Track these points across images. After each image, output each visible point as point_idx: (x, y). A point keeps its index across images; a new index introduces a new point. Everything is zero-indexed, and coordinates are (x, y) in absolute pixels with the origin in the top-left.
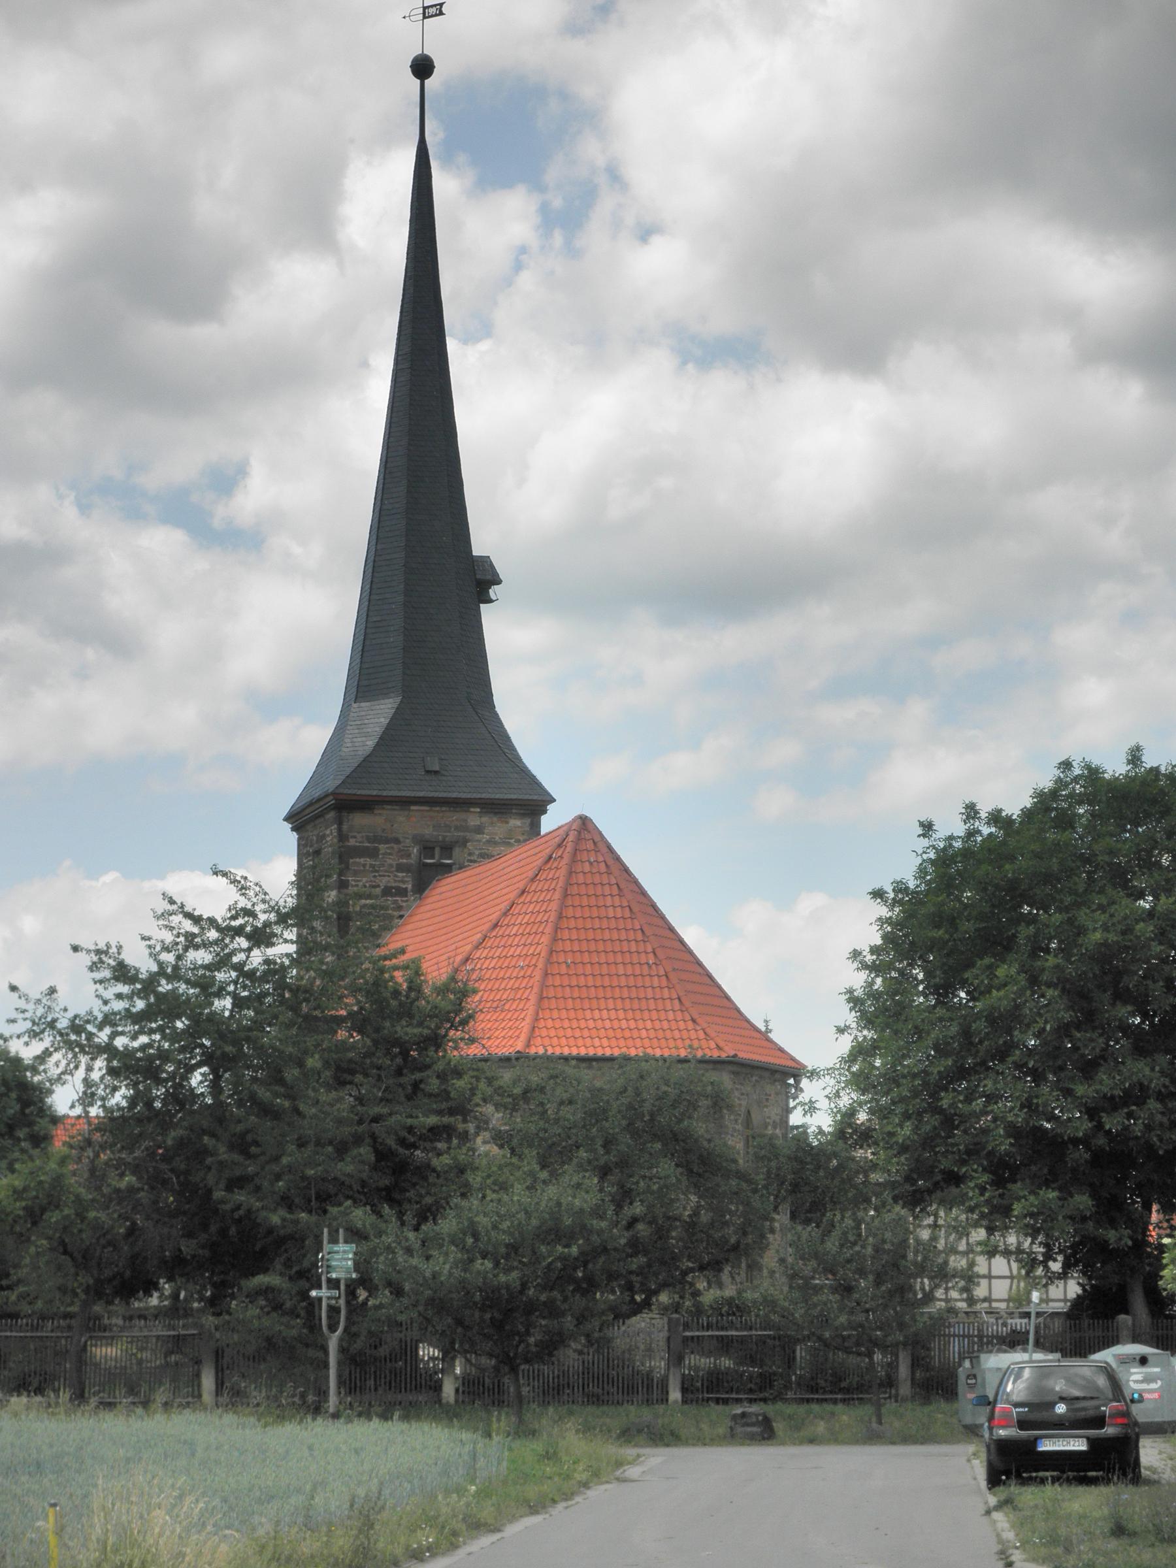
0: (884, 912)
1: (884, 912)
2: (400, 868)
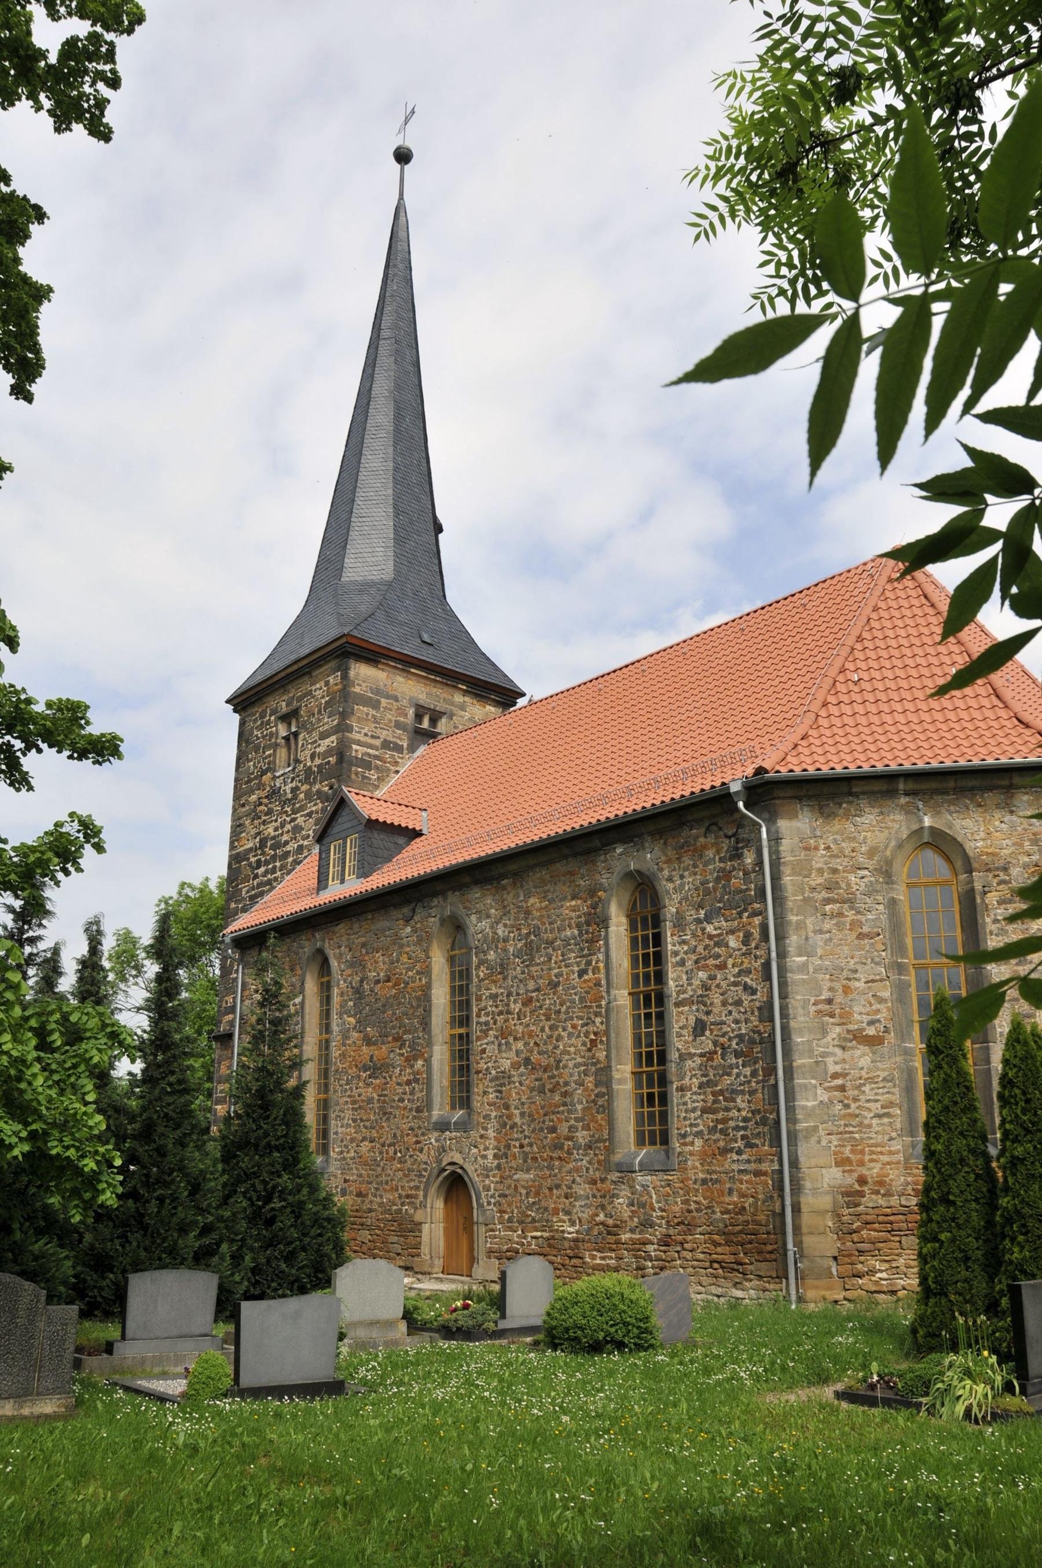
0: (148, 995)
1: (148, 995)
2: (398, 725)
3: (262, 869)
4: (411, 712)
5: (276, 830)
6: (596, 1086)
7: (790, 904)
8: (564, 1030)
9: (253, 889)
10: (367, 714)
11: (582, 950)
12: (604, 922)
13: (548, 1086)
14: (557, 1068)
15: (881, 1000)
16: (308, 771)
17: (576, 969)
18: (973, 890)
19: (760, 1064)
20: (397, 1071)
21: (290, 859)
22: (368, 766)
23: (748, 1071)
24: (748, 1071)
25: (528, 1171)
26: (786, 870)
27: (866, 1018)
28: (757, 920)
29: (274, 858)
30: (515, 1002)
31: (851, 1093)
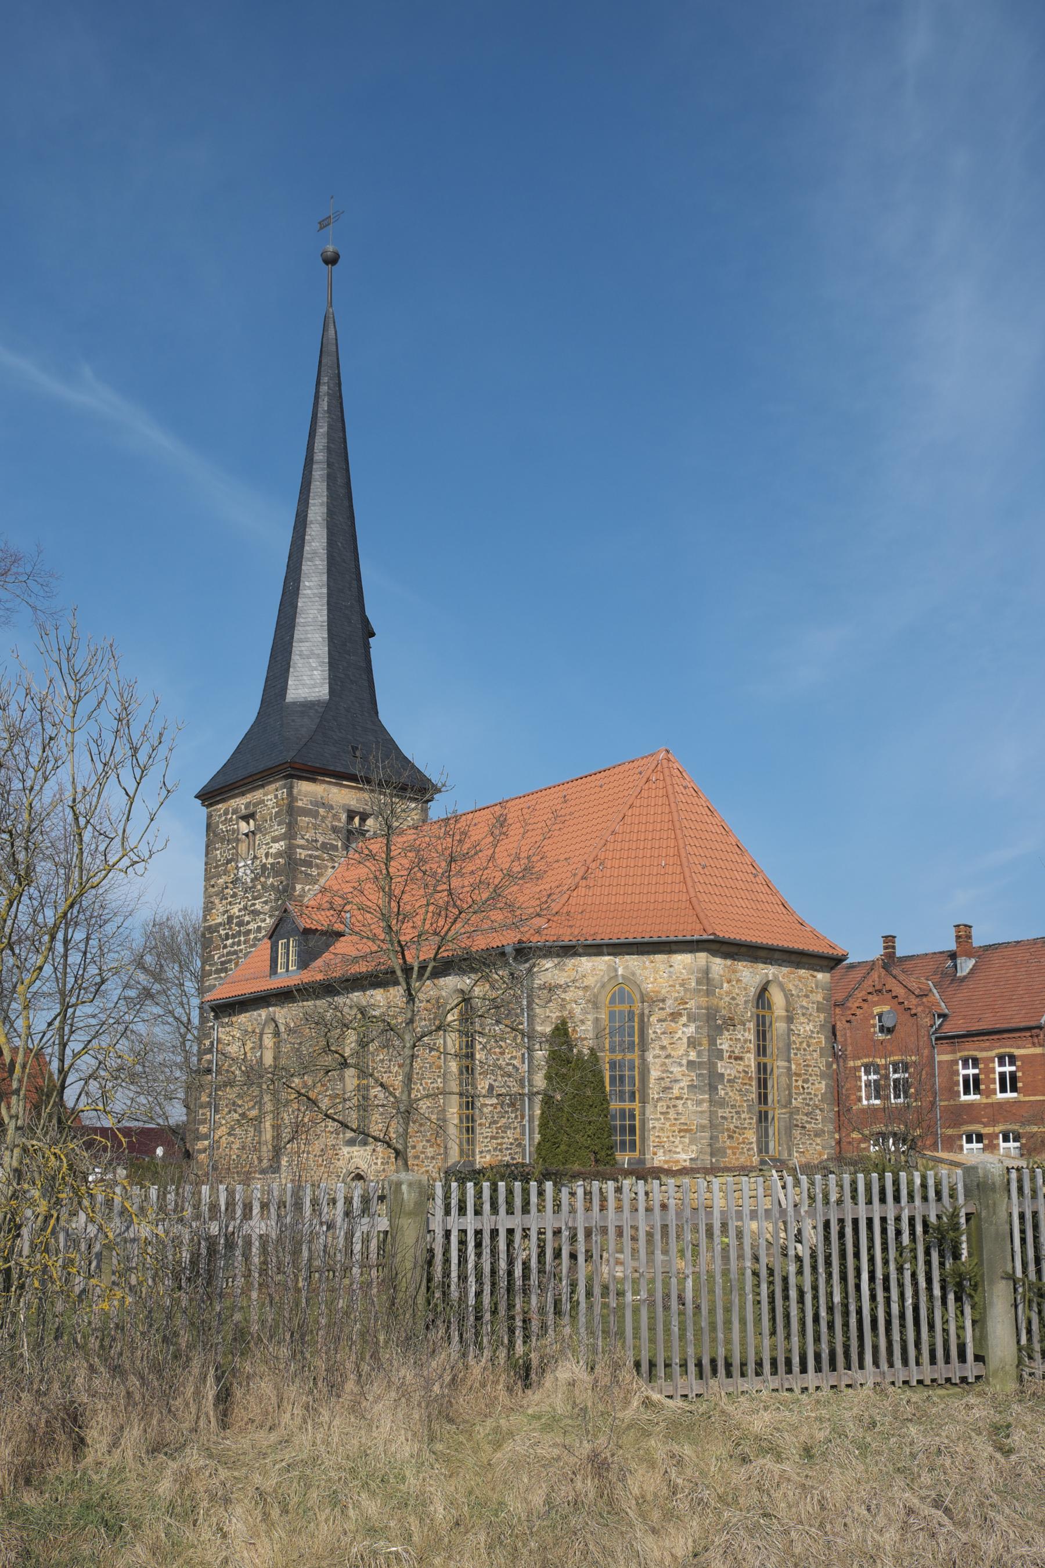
3: (230, 941)
4: (344, 817)
5: (240, 911)
9: (223, 956)
10: (308, 823)
12: (227, 1204)
16: (264, 867)
19: (518, 1113)
21: (252, 936)
22: (309, 865)
23: (513, 1115)
24: (513, 1115)
29: (239, 933)
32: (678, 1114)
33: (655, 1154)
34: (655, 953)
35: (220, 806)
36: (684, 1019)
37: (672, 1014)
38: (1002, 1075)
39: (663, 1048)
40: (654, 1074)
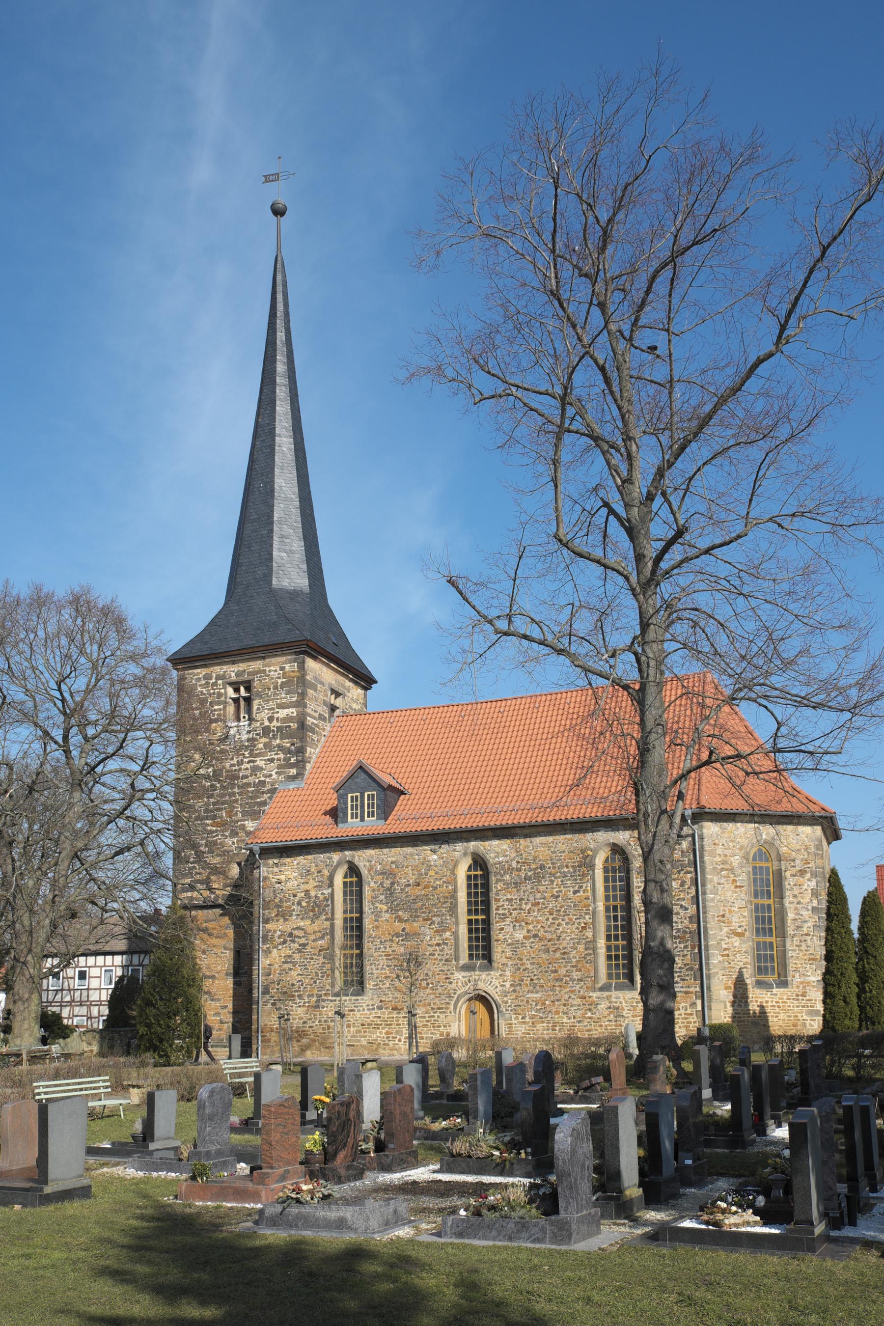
6: (586, 949)
7: (707, 870)
8: (563, 920)
11: (576, 880)
13: (551, 949)
14: (558, 940)
15: (745, 917)
17: (572, 889)
18: (781, 869)
20: (428, 938)
23: (682, 946)
24: (682, 946)
25: (537, 992)
26: (706, 854)
27: (738, 925)
28: (689, 876)
30: (526, 904)
31: (731, 958)
32: (808, 947)
33: (794, 977)
34: (786, 824)
35: (199, 670)
36: (808, 875)
37: (800, 871)
38: (771, 936)
39: (795, 896)
40: (791, 916)
